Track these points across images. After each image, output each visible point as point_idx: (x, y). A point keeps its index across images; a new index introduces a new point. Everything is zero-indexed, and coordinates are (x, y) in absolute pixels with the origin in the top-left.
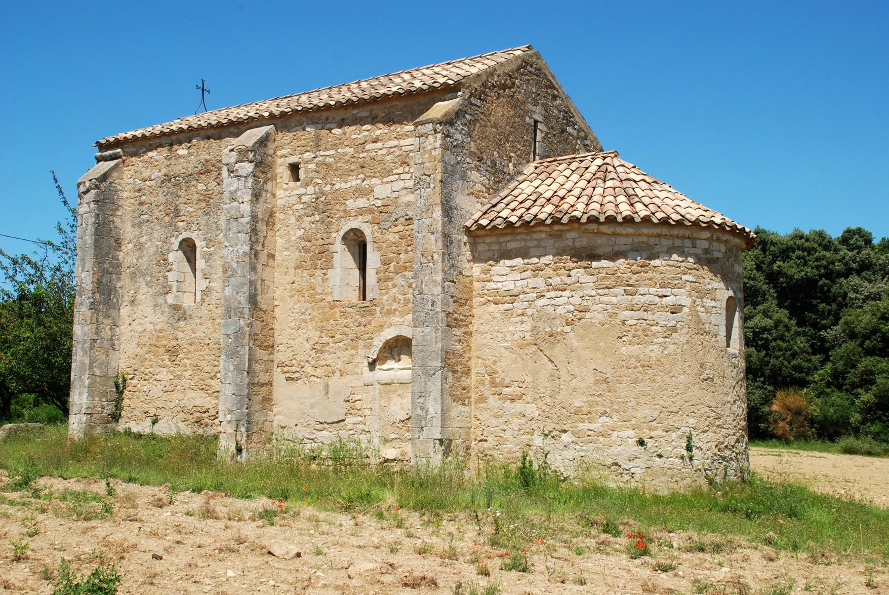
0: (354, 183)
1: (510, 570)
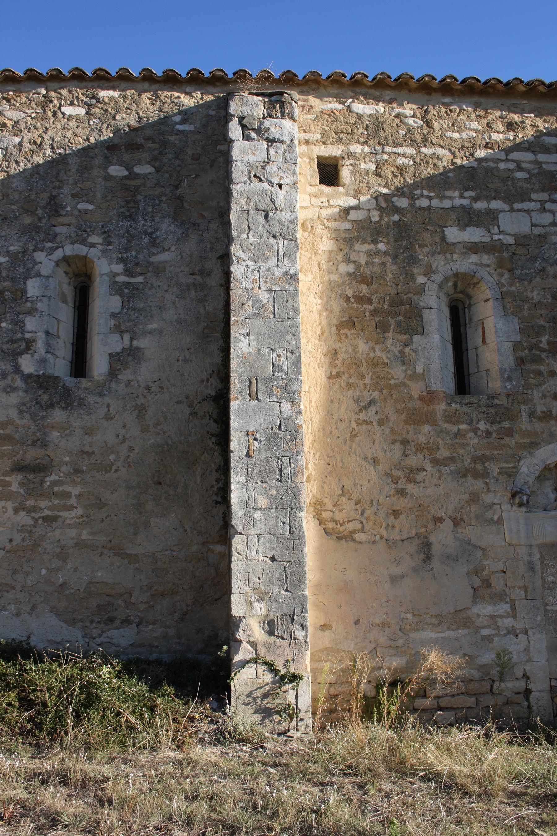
0: (458, 202)
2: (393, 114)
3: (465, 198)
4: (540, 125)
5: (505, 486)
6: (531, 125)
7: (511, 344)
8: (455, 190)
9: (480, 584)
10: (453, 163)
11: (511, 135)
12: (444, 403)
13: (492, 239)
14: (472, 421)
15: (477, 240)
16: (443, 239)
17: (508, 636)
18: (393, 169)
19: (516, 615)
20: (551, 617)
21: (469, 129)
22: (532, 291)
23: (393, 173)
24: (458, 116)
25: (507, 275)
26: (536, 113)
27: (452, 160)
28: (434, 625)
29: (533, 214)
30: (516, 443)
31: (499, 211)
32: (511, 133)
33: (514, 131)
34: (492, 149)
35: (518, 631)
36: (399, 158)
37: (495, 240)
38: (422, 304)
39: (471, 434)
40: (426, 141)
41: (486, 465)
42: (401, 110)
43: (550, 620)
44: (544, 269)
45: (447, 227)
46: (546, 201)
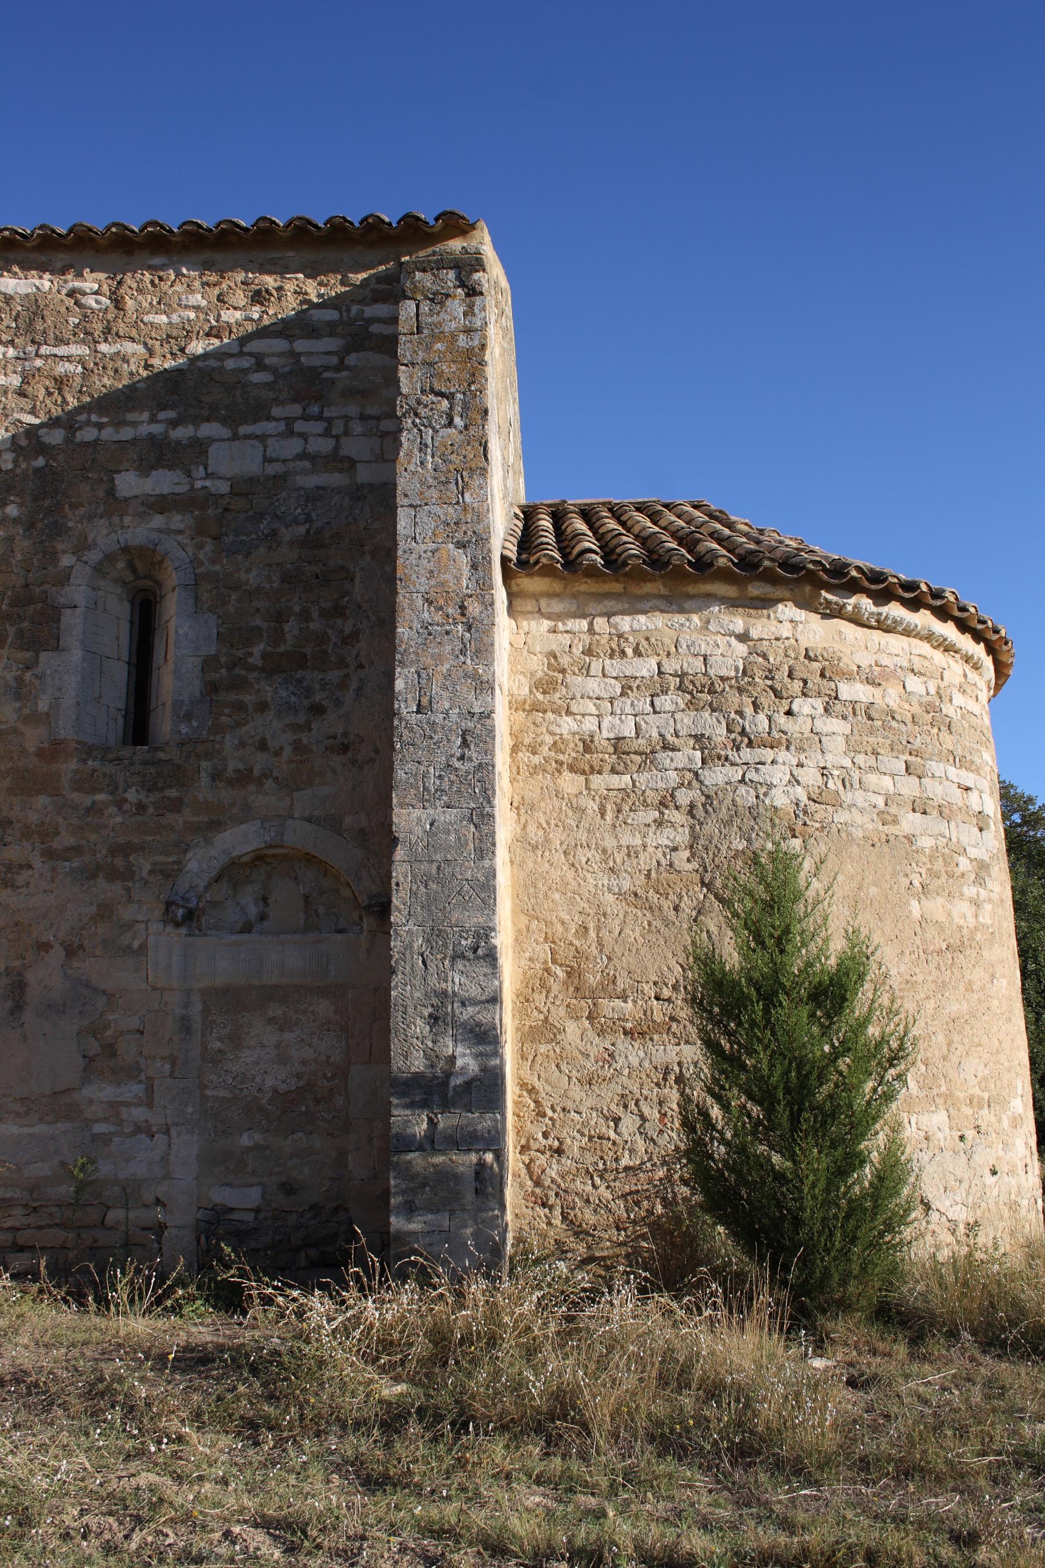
0: (145, 430)
1: (875, 1377)
2: (64, 291)
3: (158, 422)
4: (309, 290)
5: (157, 893)
6: (296, 292)
7: (200, 659)
8: (143, 411)
9: (99, 1051)
10: (147, 367)
11: (255, 312)
12: (75, 760)
13: (192, 487)
14: (117, 788)
15: (166, 491)
16: (111, 492)
17: (138, 1136)
18: (48, 383)
19: (152, 1101)
20: (211, 1107)
21: (186, 307)
22: (249, 571)
23: (47, 389)
24: (172, 286)
25: (209, 546)
26: (309, 271)
27: (146, 360)
28: (17, 1114)
29: (270, 441)
30: (185, 822)
31: (211, 440)
32: (257, 308)
33: (262, 304)
34: (218, 337)
35: (154, 1129)
36: (61, 363)
37: (198, 490)
38: (62, 600)
39: (112, 810)
40: (109, 333)
41: (131, 858)
42: (77, 284)
43: (209, 1112)
44: (274, 533)
45: (119, 472)
46: (297, 419)
